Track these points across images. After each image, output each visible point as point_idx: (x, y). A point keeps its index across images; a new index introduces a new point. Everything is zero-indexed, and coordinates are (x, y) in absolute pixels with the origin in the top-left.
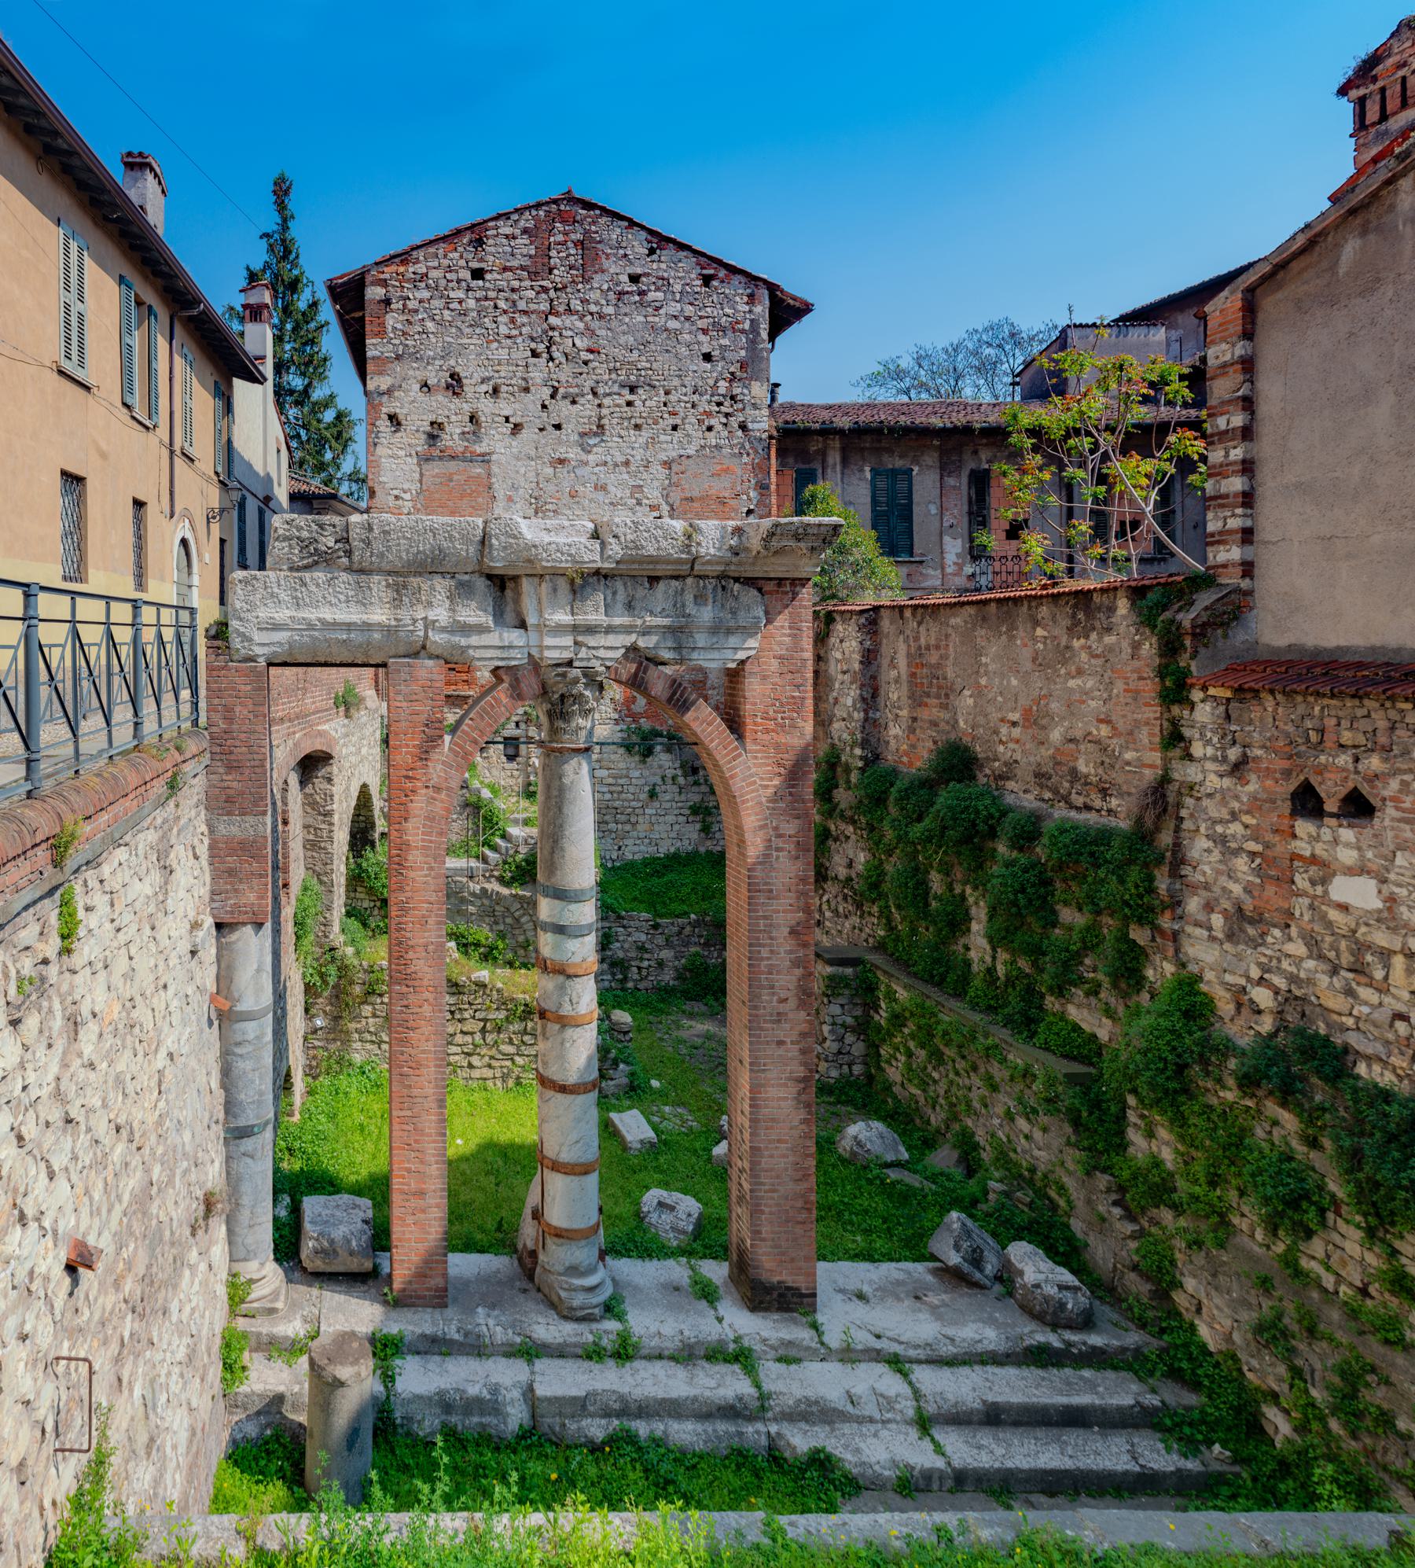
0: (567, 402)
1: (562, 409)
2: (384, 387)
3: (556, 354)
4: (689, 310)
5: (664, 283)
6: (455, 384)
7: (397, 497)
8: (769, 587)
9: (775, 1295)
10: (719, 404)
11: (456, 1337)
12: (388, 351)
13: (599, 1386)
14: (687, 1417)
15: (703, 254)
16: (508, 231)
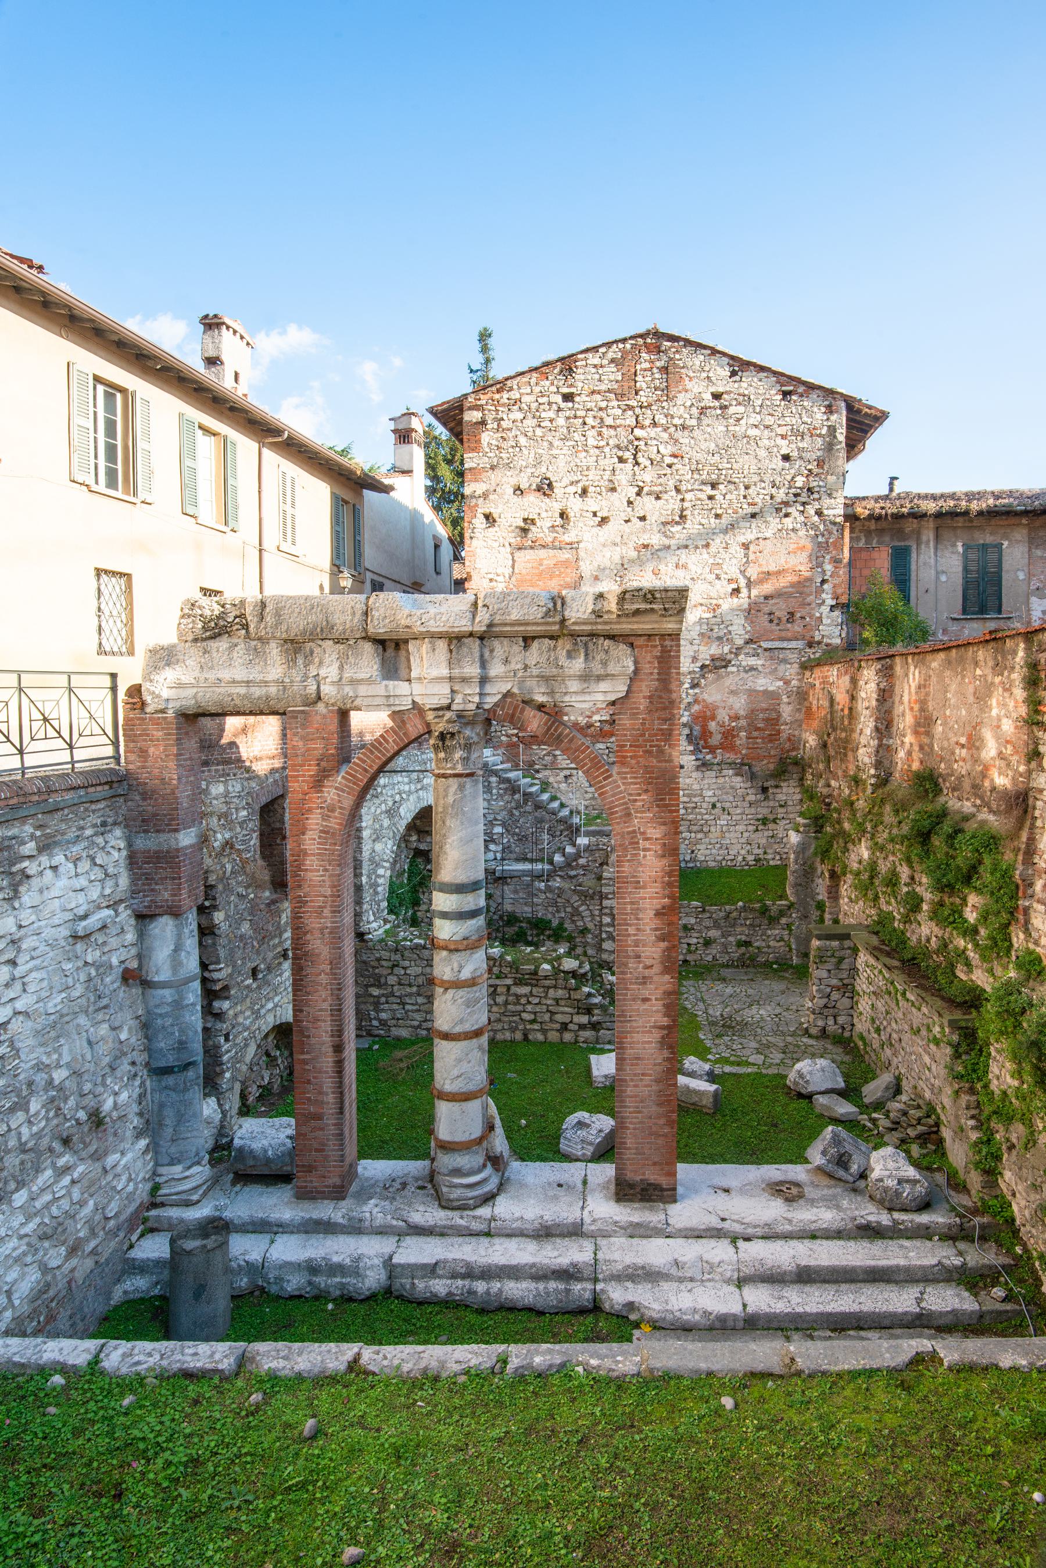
0: (652, 498)
1: (647, 505)
2: (479, 492)
3: (640, 460)
4: (769, 421)
5: (746, 400)
6: (545, 488)
7: (491, 580)
8: (640, 641)
9: (638, 1190)
10: (796, 495)
11: (341, 1221)
12: (484, 462)
13: (450, 1256)
14: (525, 1279)
15: (783, 375)
16: (596, 361)
